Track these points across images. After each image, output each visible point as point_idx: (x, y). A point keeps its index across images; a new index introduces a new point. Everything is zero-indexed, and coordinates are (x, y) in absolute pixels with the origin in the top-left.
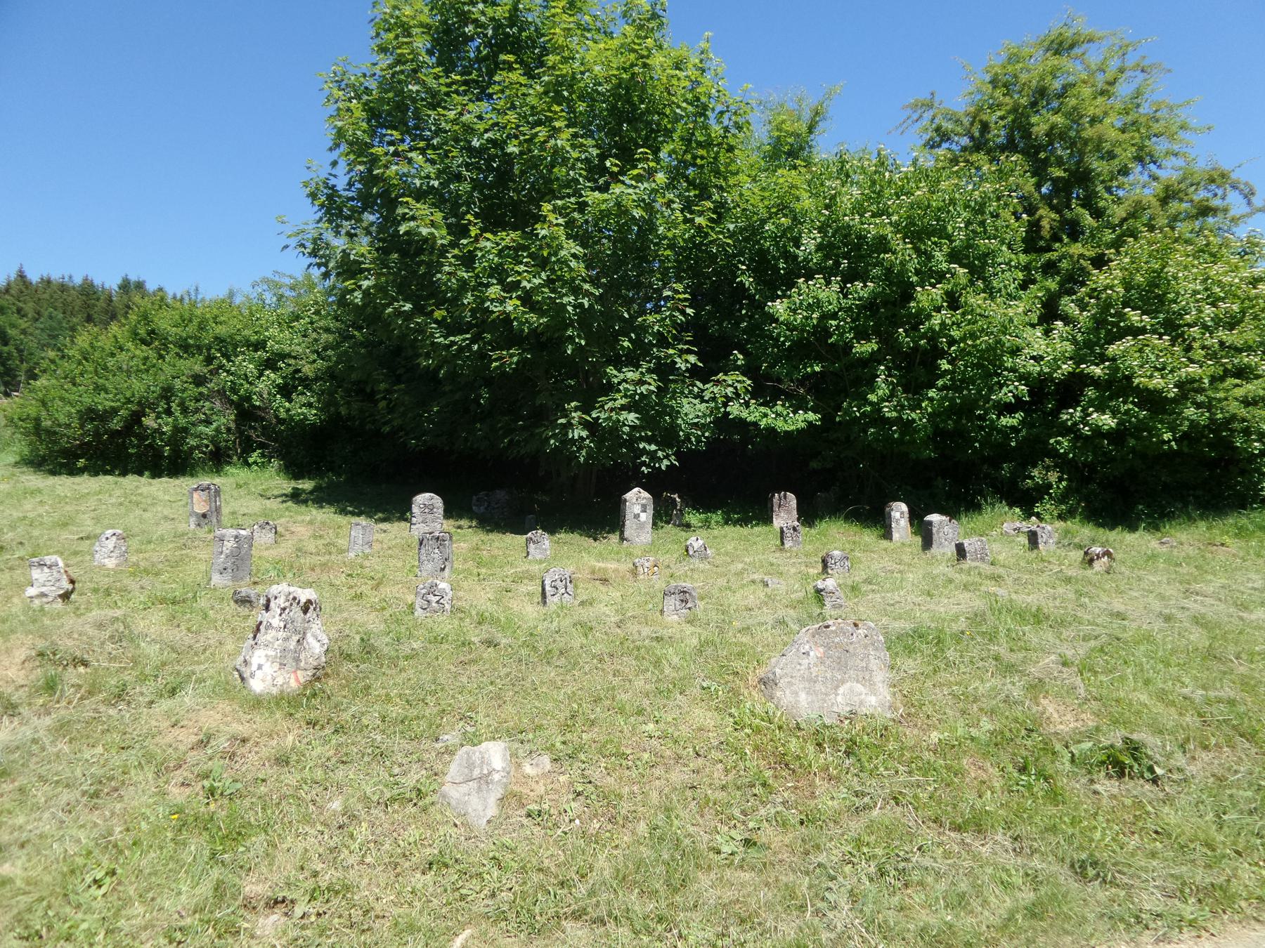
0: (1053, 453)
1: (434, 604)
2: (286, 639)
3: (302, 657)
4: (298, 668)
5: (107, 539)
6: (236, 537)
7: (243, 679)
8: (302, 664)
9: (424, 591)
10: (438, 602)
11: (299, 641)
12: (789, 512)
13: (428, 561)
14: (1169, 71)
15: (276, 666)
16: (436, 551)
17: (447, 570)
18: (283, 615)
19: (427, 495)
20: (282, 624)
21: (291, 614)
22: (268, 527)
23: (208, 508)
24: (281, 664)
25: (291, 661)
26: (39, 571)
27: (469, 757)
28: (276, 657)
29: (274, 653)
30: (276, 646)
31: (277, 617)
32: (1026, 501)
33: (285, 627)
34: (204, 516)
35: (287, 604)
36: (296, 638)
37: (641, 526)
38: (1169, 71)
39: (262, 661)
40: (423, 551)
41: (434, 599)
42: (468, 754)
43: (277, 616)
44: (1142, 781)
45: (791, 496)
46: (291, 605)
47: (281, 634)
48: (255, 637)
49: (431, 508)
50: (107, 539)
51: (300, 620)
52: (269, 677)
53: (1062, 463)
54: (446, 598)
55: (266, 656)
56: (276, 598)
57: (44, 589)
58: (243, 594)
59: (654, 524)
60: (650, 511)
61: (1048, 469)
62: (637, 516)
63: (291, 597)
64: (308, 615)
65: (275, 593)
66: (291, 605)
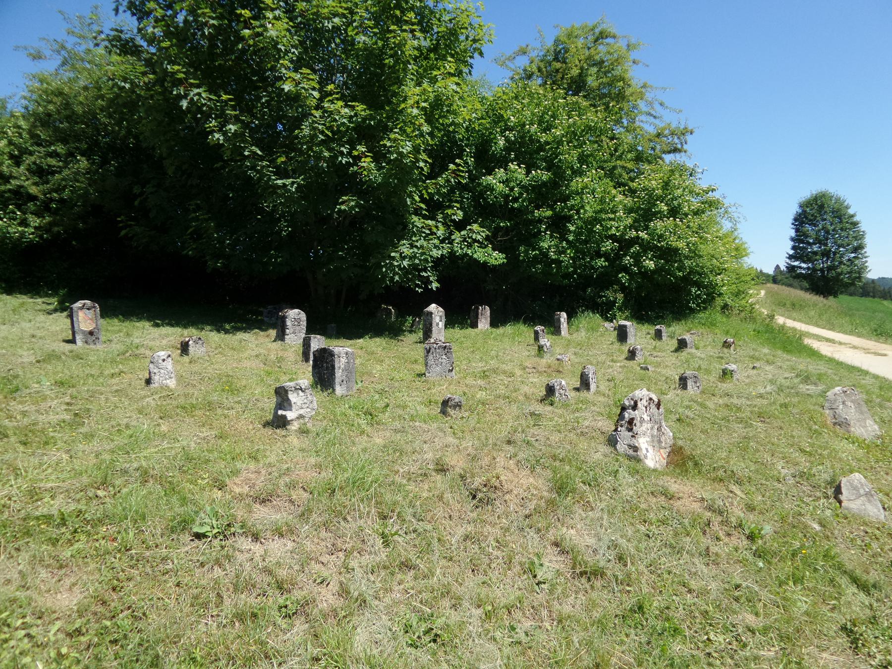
0: (618, 282)
2: (652, 428)
3: (663, 439)
4: (661, 448)
5: (164, 360)
6: (347, 354)
8: (663, 445)
12: (486, 319)
14: (647, 66)
16: (444, 357)
19: (297, 311)
22: (200, 342)
23: (94, 326)
26: (295, 395)
27: (851, 485)
32: (605, 311)
34: (91, 333)
37: (440, 330)
38: (647, 66)
42: (848, 481)
45: (487, 308)
47: (649, 426)
49: (298, 321)
50: (164, 360)
53: (623, 288)
56: (641, 400)
57: (302, 412)
58: (457, 400)
59: (446, 327)
60: (444, 320)
61: (615, 291)
62: (438, 324)
65: (640, 396)
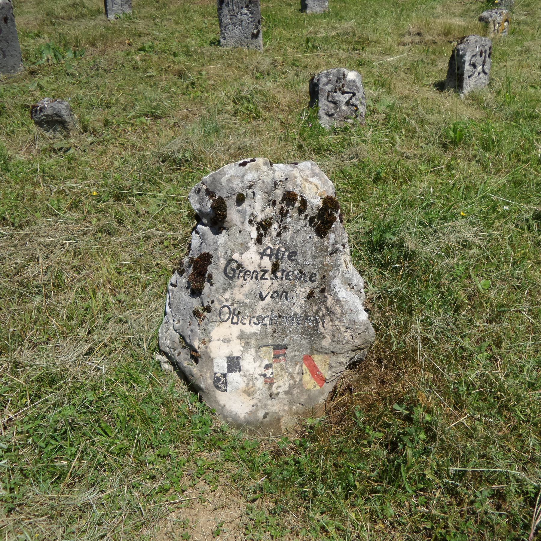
1: (344, 108)
7: (194, 389)
8: (326, 343)
9: (328, 88)
10: (348, 103)
11: (310, 295)
13: (234, 24)
15: (268, 354)
16: (245, 11)
17: (261, 35)
18: (267, 241)
20: (267, 263)
21: (287, 236)
24: (276, 347)
25: (296, 337)
28: (264, 334)
29: (256, 329)
30: (259, 313)
31: (253, 248)
33: (275, 268)
35: (270, 211)
36: (303, 290)
39: (236, 349)
40: (225, 11)
41: (343, 98)
43: (252, 244)
44: (464, 105)
46: (283, 214)
48: (196, 292)
51: (310, 250)
52: (260, 383)
54: (359, 95)
55: (242, 336)
56: (241, 199)
58: (49, 112)
63: (279, 192)
64: (332, 237)
65: (238, 186)
66: (283, 214)
